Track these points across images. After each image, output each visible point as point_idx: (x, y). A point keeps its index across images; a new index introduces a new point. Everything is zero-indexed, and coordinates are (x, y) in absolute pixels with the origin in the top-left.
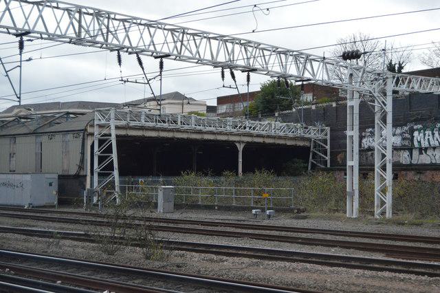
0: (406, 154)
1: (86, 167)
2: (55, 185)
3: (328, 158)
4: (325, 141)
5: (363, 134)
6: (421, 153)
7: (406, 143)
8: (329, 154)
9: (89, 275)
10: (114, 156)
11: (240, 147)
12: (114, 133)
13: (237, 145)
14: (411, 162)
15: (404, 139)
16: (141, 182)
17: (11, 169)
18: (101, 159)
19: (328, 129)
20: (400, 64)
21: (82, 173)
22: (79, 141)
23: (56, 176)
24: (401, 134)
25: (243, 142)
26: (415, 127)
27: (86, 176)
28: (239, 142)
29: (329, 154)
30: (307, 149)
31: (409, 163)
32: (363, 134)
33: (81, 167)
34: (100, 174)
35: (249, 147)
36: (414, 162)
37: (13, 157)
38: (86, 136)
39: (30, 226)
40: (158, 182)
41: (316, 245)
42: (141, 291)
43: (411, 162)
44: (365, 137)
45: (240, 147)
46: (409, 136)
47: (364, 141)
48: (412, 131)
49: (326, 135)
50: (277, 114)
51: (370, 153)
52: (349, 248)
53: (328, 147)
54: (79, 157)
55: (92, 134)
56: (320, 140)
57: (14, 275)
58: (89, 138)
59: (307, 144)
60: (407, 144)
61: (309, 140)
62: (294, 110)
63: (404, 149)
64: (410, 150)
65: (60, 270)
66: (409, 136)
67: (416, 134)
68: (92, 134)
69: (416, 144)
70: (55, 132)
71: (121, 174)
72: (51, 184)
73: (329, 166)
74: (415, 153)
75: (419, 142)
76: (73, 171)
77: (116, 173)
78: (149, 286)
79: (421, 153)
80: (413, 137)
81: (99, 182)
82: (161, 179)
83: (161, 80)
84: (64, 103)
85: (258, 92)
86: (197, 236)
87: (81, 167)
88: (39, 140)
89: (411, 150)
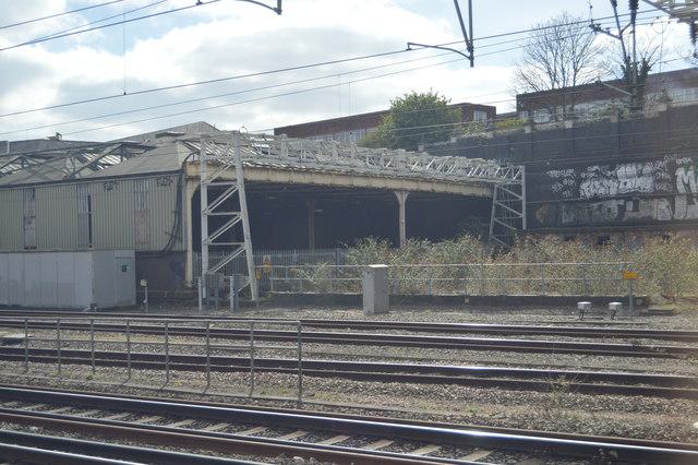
0: (664, 205)
1: (186, 237)
2: (131, 269)
3: (523, 215)
4: (517, 188)
5: (583, 175)
6: (690, 202)
7: (664, 187)
8: (524, 208)
9: (344, 443)
10: (243, 215)
11: (402, 199)
12: (239, 175)
13: (398, 195)
14: (672, 217)
15: (658, 181)
16: (267, 260)
17: (27, 245)
18: (214, 223)
19: (522, 168)
20: (645, 63)
21: (177, 247)
22: (170, 193)
23: (132, 254)
24: (653, 174)
25: (406, 190)
26: (679, 162)
27: (186, 251)
28: (400, 190)
29: (524, 208)
30: (487, 201)
31: (669, 218)
32: (583, 175)
33: (176, 235)
34: (211, 249)
35: (415, 198)
36: (679, 216)
37: (30, 223)
38: (183, 183)
39: (639, 372)
40: (289, 261)
41: (595, 354)
42: (375, 460)
43: (672, 217)
44: (585, 180)
45: (402, 199)
46: (668, 177)
47: (584, 186)
48: (673, 168)
49: (519, 178)
50: (421, 148)
51: (595, 205)
52: (508, 350)
53: (523, 197)
54: (170, 220)
55: (197, 178)
56: (505, 187)
57: (38, 432)
58: (189, 184)
59: (484, 192)
60: (664, 188)
61: (490, 186)
62: (453, 140)
63: (659, 198)
64: (671, 197)
65: (42, 409)
66: (668, 177)
67: (680, 172)
68: (197, 178)
69: (681, 188)
70: (118, 177)
71: (256, 248)
72: (124, 269)
73: (524, 228)
74: (680, 203)
75: (687, 185)
76: (159, 243)
77: (247, 245)
78: (372, 449)
79: (690, 202)
80: (675, 178)
81: (212, 263)
82: (295, 255)
83: (633, 32)
84: (15, 143)
85: (385, 113)
86: (45, 331)
87: (176, 235)
88: (85, 191)
89: (671, 197)
